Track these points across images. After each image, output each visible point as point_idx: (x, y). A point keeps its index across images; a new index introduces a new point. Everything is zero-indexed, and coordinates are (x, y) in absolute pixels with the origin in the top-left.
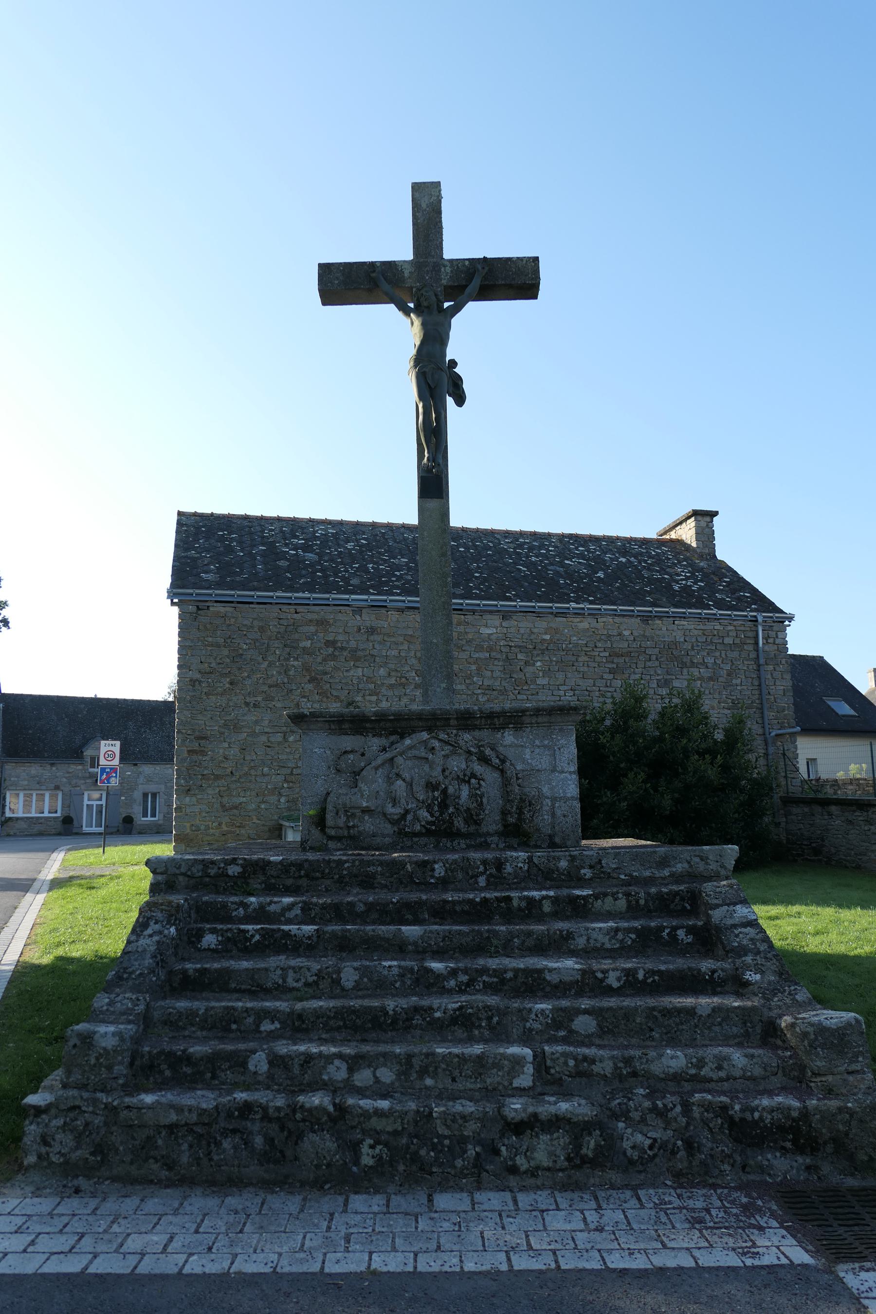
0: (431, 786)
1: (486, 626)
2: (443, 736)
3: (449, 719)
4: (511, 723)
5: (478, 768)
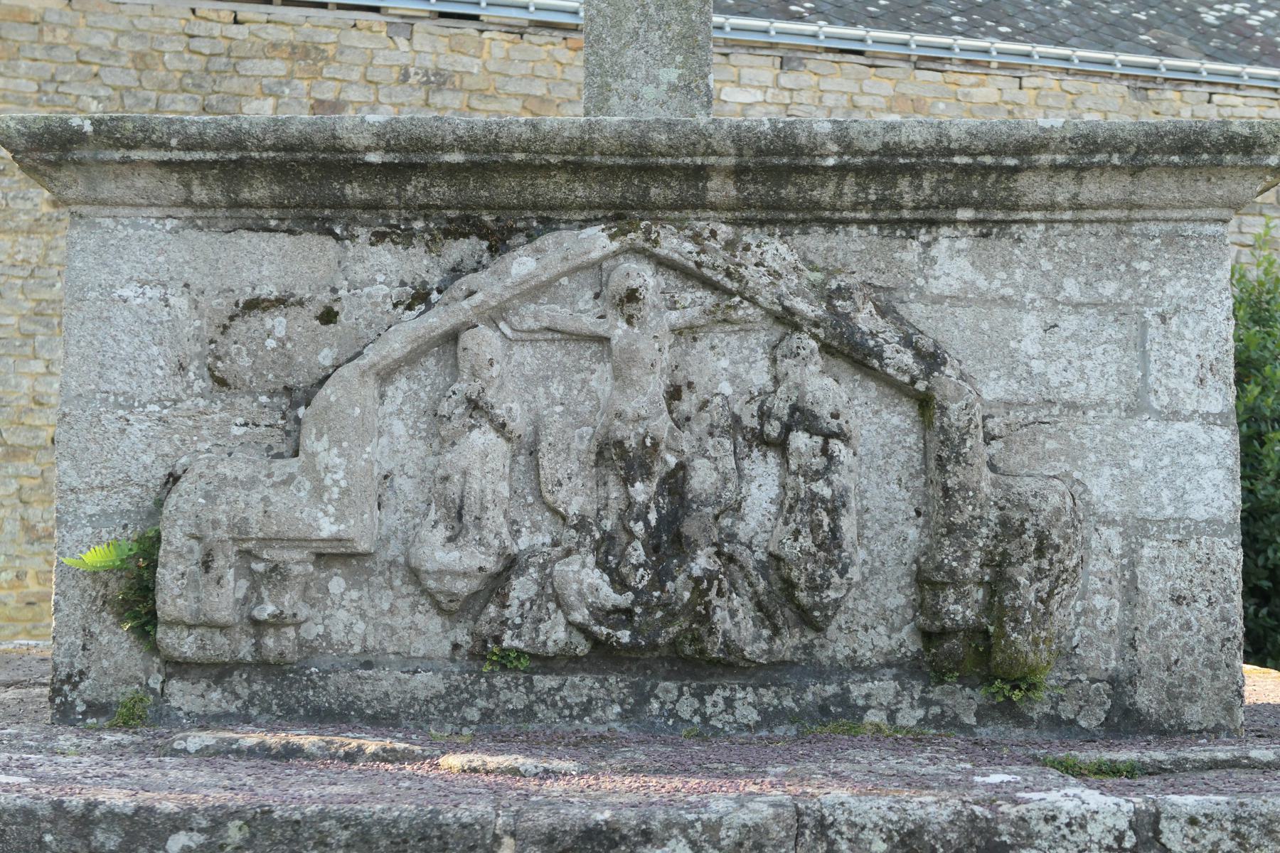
0: (618, 458)
1: (738, 83)
2: (673, 244)
3: (700, 173)
4: (964, 203)
5: (825, 387)
